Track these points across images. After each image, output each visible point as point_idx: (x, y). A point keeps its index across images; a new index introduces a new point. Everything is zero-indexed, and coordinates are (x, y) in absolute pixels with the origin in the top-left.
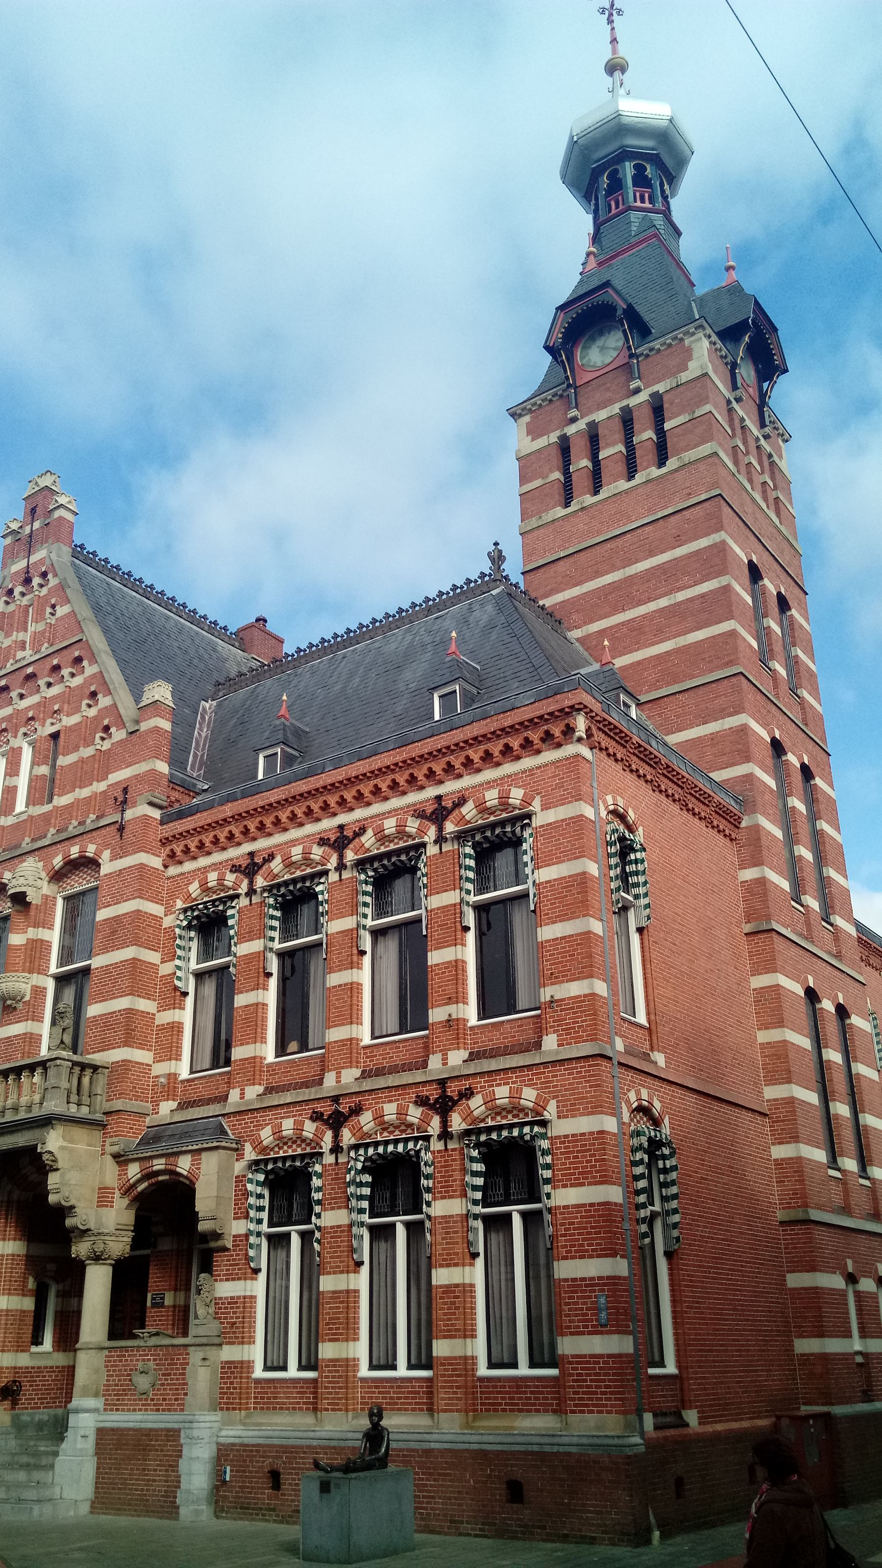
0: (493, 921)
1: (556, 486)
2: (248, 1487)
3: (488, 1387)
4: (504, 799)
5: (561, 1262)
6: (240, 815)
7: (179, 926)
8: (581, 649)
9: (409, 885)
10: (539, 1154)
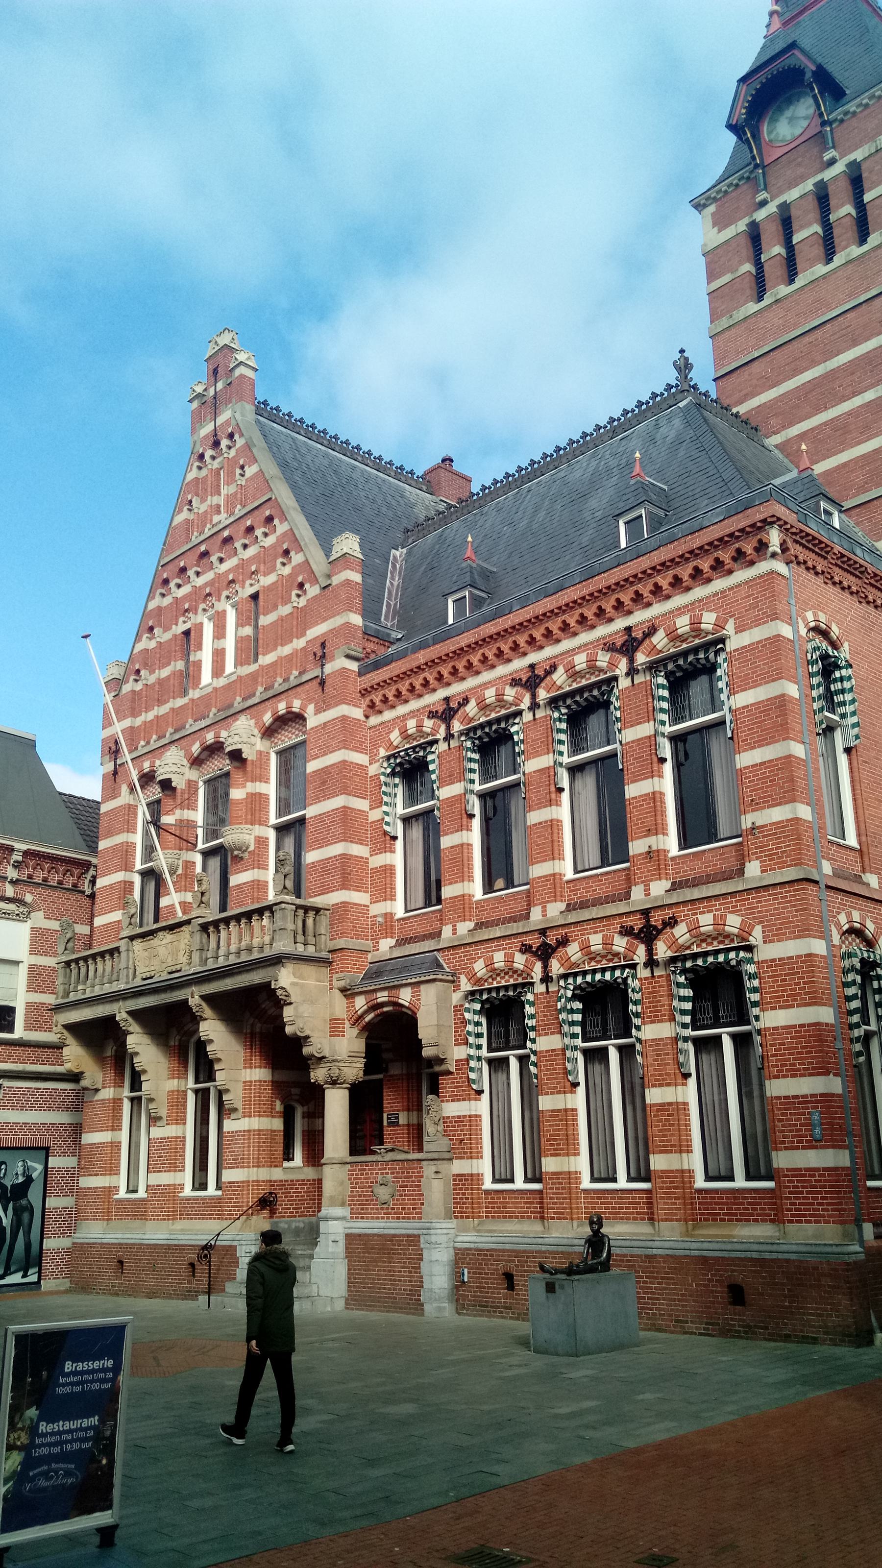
0: (691, 752)
1: (747, 280)
2: (484, 1288)
3: (706, 1198)
4: (695, 625)
5: (773, 1081)
6: (433, 661)
7: (383, 774)
8: (781, 456)
9: (603, 719)
10: (746, 978)
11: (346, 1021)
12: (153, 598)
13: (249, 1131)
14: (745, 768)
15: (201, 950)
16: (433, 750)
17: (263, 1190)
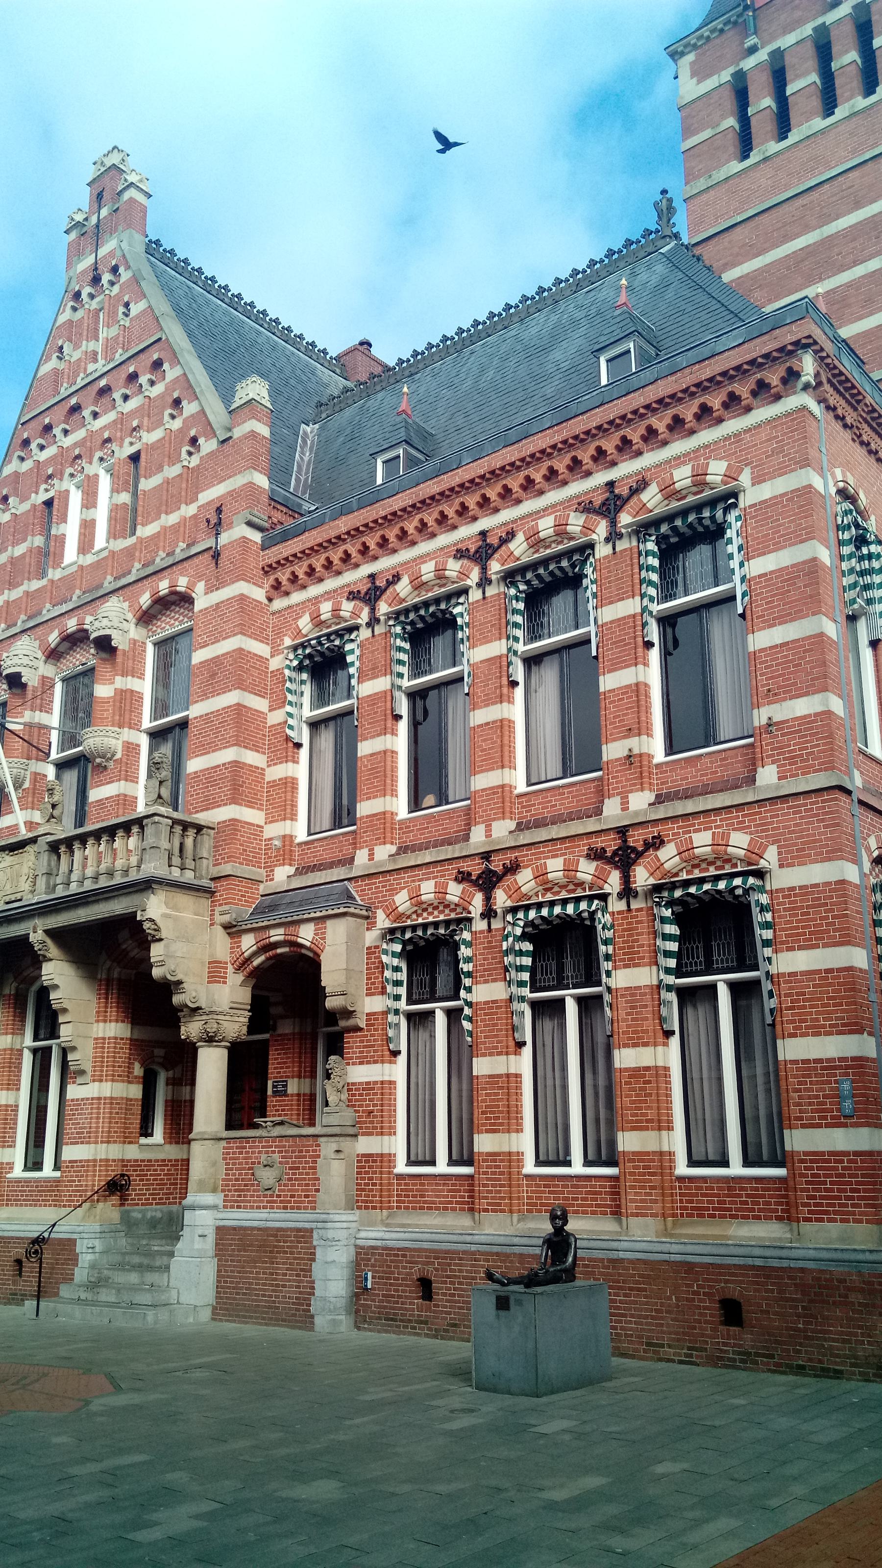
0: (681, 635)
2: (393, 1296)
7: (288, 667)
11: (229, 965)
12: (10, 462)
13: (99, 1099)
14: (761, 650)
15: (49, 874)
16: (352, 637)
17: (113, 1171)
